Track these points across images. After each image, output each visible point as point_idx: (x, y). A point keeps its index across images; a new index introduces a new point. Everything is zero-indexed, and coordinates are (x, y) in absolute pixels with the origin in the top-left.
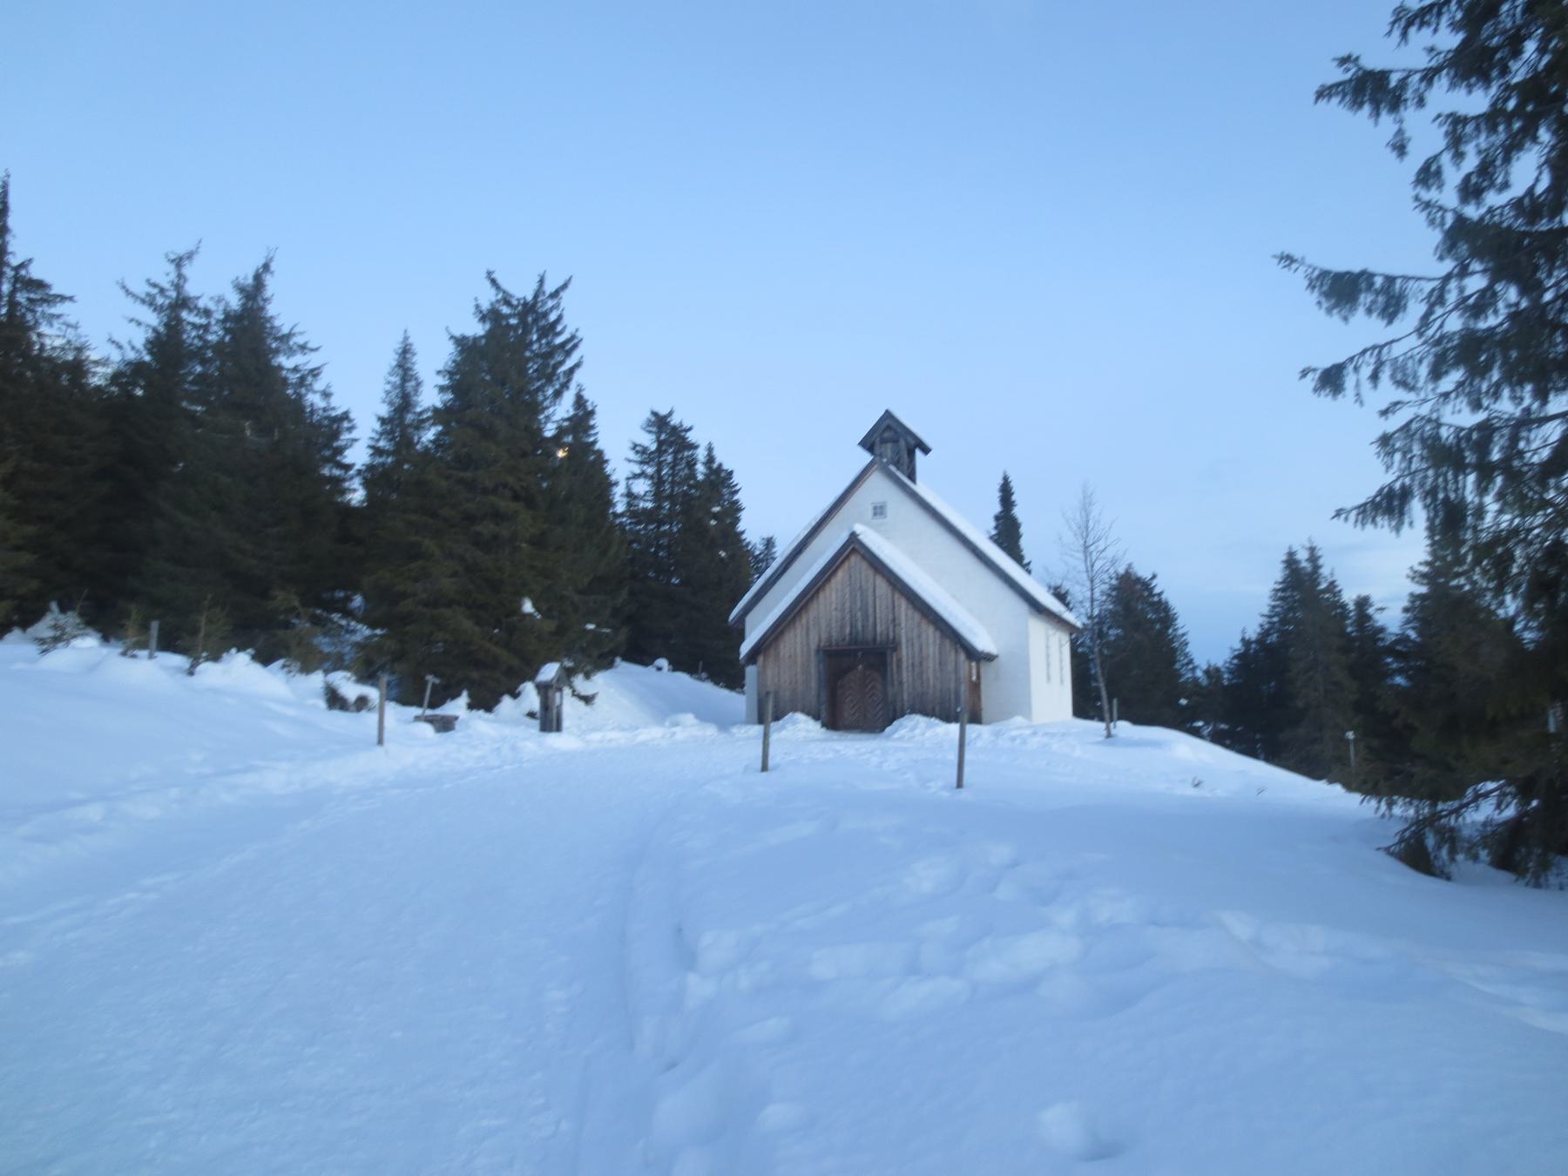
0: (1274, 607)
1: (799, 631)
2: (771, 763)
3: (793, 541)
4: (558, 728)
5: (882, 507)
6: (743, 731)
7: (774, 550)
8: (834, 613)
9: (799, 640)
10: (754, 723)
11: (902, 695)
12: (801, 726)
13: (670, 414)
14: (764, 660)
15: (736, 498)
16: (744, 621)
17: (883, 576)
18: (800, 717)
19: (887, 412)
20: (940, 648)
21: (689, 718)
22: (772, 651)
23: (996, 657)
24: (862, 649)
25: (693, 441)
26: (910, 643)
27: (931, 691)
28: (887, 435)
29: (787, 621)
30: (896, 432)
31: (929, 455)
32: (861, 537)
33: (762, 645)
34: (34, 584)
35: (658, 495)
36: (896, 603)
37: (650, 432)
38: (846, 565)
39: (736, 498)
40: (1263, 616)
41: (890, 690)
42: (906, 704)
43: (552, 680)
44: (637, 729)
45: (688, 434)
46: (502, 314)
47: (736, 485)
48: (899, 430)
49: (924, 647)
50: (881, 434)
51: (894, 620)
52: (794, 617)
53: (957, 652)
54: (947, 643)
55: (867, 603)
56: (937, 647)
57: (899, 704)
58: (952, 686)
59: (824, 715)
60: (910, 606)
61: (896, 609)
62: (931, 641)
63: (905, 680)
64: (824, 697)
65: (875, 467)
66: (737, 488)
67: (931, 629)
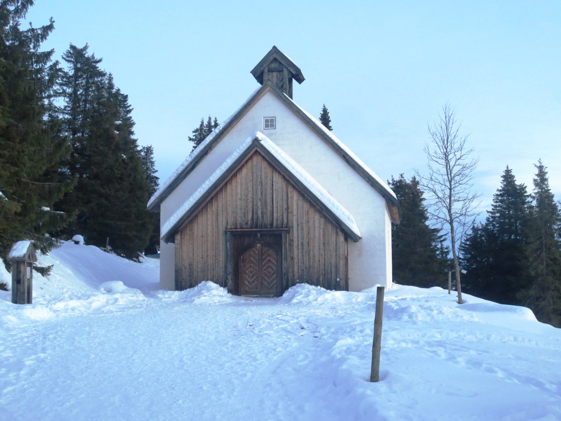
0: (496, 206)
1: (209, 216)
2: (383, 367)
4: (29, 301)
5: (272, 121)
6: (167, 296)
7: (152, 156)
8: (239, 202)
9: (209, 223)
11: (293, 267)
12: (214, 292)
13: (86, 48)
15: (129, 116)
16: (159, 207)
17: (279, 173)
18: (211, 284)
19: (274, 47)
20: (324, 231)
21: (119, 285)
22: (188, 232)
23: (360, 238)
24: (260, 231)
25: (102, 70)
26: (300, 227)
27: (316, 265)
28: (273, 66)
29: (201, 207)
30: (280, 63)
31: (303, 83)
32: (262, 142)
33: (180, 227)
35: (74, 111)
36: (290, 194)
37: (69, 61)
38: (250, 164)
39: (129, 116)
40: (488, 212)
41: (285, 264)
42: (296, 274)
43: (24, 256)
44: (89, 297)
45: (98, 65)
47: (130, 106)
48: (283, 62)
49: (311, 231)
50: (268, 66)
52: (212, 199)
53: (337, 233)
54: (330, 227)
55: (266, 195)
56: (322, 230)
57: (290, 275)
58: (333, 261)
59: (230, 282)
60: (301, 198)
61: (289, 200)
62: (317, 224)
63: (295, 256)
64: (230, 269)
65: (267, 89)
66: (131, 108)
67: (317, 217)
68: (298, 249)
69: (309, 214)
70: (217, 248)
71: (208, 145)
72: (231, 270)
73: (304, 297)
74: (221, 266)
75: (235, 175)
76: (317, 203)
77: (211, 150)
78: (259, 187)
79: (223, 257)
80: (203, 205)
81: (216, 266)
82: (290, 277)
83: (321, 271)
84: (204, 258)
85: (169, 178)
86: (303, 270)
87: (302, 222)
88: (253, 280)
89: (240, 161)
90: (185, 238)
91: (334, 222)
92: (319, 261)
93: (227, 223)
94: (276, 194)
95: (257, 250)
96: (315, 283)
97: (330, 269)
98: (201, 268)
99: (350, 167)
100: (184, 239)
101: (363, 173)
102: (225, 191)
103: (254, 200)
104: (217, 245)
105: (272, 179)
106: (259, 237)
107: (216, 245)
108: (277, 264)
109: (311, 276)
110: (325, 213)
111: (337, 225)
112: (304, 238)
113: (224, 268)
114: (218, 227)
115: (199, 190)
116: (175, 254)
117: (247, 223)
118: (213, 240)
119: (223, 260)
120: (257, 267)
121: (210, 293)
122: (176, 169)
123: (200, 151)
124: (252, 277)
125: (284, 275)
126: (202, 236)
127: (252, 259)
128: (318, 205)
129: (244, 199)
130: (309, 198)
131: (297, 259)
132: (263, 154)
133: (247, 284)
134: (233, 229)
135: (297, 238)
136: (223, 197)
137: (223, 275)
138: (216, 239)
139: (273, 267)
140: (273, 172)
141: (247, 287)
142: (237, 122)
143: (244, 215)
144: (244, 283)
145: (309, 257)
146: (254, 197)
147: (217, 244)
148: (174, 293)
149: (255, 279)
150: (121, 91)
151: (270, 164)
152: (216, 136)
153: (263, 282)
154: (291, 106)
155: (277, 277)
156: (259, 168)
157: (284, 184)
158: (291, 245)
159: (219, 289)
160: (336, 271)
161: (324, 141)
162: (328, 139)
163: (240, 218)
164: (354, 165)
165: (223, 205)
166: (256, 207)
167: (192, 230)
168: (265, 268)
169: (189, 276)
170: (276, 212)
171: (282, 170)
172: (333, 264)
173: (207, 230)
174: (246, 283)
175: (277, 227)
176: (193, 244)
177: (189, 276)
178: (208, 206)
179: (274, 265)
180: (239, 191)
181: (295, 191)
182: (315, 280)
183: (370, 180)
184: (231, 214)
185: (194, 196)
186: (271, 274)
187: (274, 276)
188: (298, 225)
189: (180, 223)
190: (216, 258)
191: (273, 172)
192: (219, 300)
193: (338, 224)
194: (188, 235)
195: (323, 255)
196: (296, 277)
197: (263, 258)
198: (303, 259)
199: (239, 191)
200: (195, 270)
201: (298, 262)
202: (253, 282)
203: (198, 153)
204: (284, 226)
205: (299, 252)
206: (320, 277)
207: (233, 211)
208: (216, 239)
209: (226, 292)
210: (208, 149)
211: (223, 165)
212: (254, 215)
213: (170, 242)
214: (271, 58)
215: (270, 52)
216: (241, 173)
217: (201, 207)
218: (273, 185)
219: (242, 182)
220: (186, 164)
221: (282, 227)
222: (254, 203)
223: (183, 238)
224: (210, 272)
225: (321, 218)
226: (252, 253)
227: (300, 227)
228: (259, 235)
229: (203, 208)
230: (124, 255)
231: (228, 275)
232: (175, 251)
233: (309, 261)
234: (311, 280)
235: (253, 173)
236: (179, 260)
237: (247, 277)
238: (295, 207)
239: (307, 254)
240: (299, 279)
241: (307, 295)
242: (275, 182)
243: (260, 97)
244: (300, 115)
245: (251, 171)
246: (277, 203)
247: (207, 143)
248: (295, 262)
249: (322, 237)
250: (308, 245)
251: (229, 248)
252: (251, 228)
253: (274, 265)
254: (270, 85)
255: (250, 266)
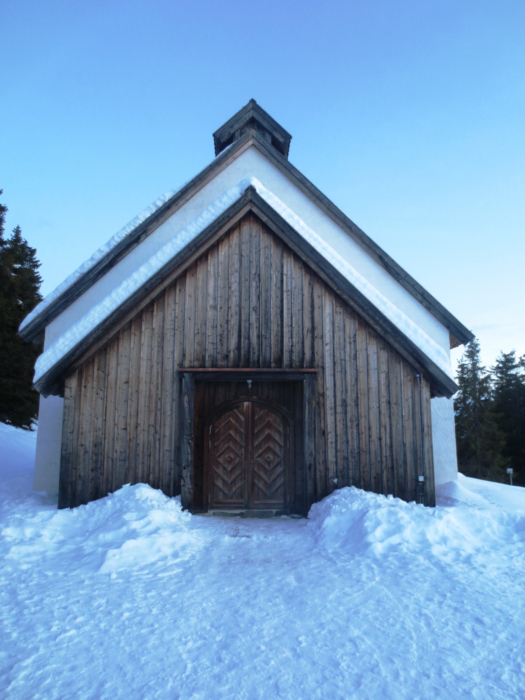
1: (145, 339)
3: (129, 224)
8: (210, 313)
9: (144, 354)
10: (44, 502)
11: (325, 452)
14: (80, 384)
17: (297, 258)
19: (253, 101)
20: (388, 377)
27: (374, 446)
29: (128, 320)
34: (216, 444)
36: (317, 301)
38: (235, 238)
41: (309, 444)
42: (332, 467)
46: (81, 504)
47: (39, 261)
48: (265, 124)
49: (362, 376)
51: (313, 329)
52: (152, 304)
53: (415, 381)
55: (267, 301)
56: (383, 376)
57: (320, 467)
58: (408, 439)
59: (187, 485)
60: (339, 309)
61: (317, 312)
62: (373, 364)
63: (330, 427)
65: (251, 143)
66: (39, 263)
67: (373, 348)
68: (335, 412)
69: (357, 341)
70: (159, 407)
71: (140, 225)
72: (190, 458)
73: (389, 534)
74: (167, 447)
75: (204, 257)
76: (377, 318)
77: (147, 236)
78: (254, 284)
79: (171, 427)
80: (132, 315)
81: (155, 447)
82: (318, 473)
83: (384, 459)
84: (128, 429)
85: (66, 281)
86: (346, 459)
87: (343, 358)
88: (233, 477)
89: (216, 229)
90: (89, 385)
91: (411, 359)
92: (380, 439)
93: (184, 355)
94: (288, 299)
95: (242, 414)
96: (373, 486)
97: (402, 457)
98: (121, 452)
99: (390, 277)
100: (85, 387)
101: (413, 287)
102: (180, 290)
103: (242, 310)
104: (159, 402)
105: (279, 269)
106: (250, 386)
107: (157, 402)
108: (285, 442)
109: (364, 472)
110: (391, 340)
111: (417, 365)
112: (346, 391)
113: (173, 453)
114: (162, 362)
115: (125, 284)
116: (64, 420)
117: (227, 357)
118: (150, 391)
119: (171, 436)
120: (243, 450)
121: (145, 520)
122: (80, 264)
123: (126, 235)
124: (231, 471)
125: (310, 469)
126: (127, 382)
127: (232, 432)
128: (377, 322)
129: (221, 308)
130: (356, 307)
131: (334, 434)
132: (264, 219)
133: (221, 486)
134: (196, 367)
135: (333, 389)
136: (177, 301)
137: (171, 469)
138: (157, 389)
139: (277, 449)
140: (282, 256)
141: (221, 493)
142: (195, 191)
143: (220, 340)
144: (214, 484)
145: (358, 429)
146: (243, 304)
147: (160, 399)
148: (51, 517)
149: (237, 477)
150: (28, 243)
151: (278, 241)
152: (157, 211)
153: (256, 481)
154: (290, 172)
155: (284, 470)
156: (254, 246)
157: (306, 280)
158: (321, 405)
159: (165, 507)
160: (415, 461)
161: (345, 231)
162: (353, 228)
163: (211, 346)
164: (397, 273)
165: (175, 317)
166: (247, 324)
167: (105, 367)
168: (260, 451)
169: (92, 470)
170: (289, 335)
171: (303, 251)
172: (408, 445)
173: (139, 368)
174: (219, 483)
175: (291, 366)
176: (105, 399)
177: (92, 470)
178: (144, 318)
179: (280, 446)
180: (211, 290)
181: (327, 295)
182: (373, 480)
183: (425, 299)
184: (192, 337)
185: (114, 295)
186: (272, 466)
187: (280, 469)
188: (334, 363)
189: (78, 353)
190: (156, 430)
191: (282, 256)
192: (173, 545)
193: (419, 362)
194: (95, 379)
195: (388, 427)
196: (331, 474)
197: (256, 431)
198: (346, 433)
199: (211, 290)
200: (108, 457)
201: (336, 440)
202: (234, 482)
203: (122, 239)
204: (305, 365)
205: (338, 419)
206: (382, 472)
207: (196, 332)
208: (157, 389)
209: (179, 508)
210: (140, 233)
211: (179, 236)
212: (243, 340)
213: (55, 394)
214: (248, 116)
215: (245, 108)
216: (216, 255)
217: (128, 320)
218: (282, 281)
219: (218, 273)
220: (99, 257)
221: (303, 367)
222: (243, 317)
223: (83, 384)
224: (141, 461)
225: (382, 350)
226: (231, 419)
227: (338, 368)
228: (249, 381)
229: (131, 322)
230: (10, 422)
231: (185, 468)
232: (64, 414)
233: (359, 439)
234: (364, 480)
235: (241, 256)
236: (72, 432)
237: (220, 471)
238: (328, 327)
239: (355, 424)
240: (337, 477)
241: (398, 529)
242: (286, 275)
243: (238, 153)
244: (306, 187)
245: (237, 251)
246: (292, 318)
247: (141, 222)
248: (329, 441)
249: (383, 388)
250: (357, 405)
251: (187, 410)
252: (237, 366)
253: (280, 446)
254: (255, 136)
255: (229, 447)
